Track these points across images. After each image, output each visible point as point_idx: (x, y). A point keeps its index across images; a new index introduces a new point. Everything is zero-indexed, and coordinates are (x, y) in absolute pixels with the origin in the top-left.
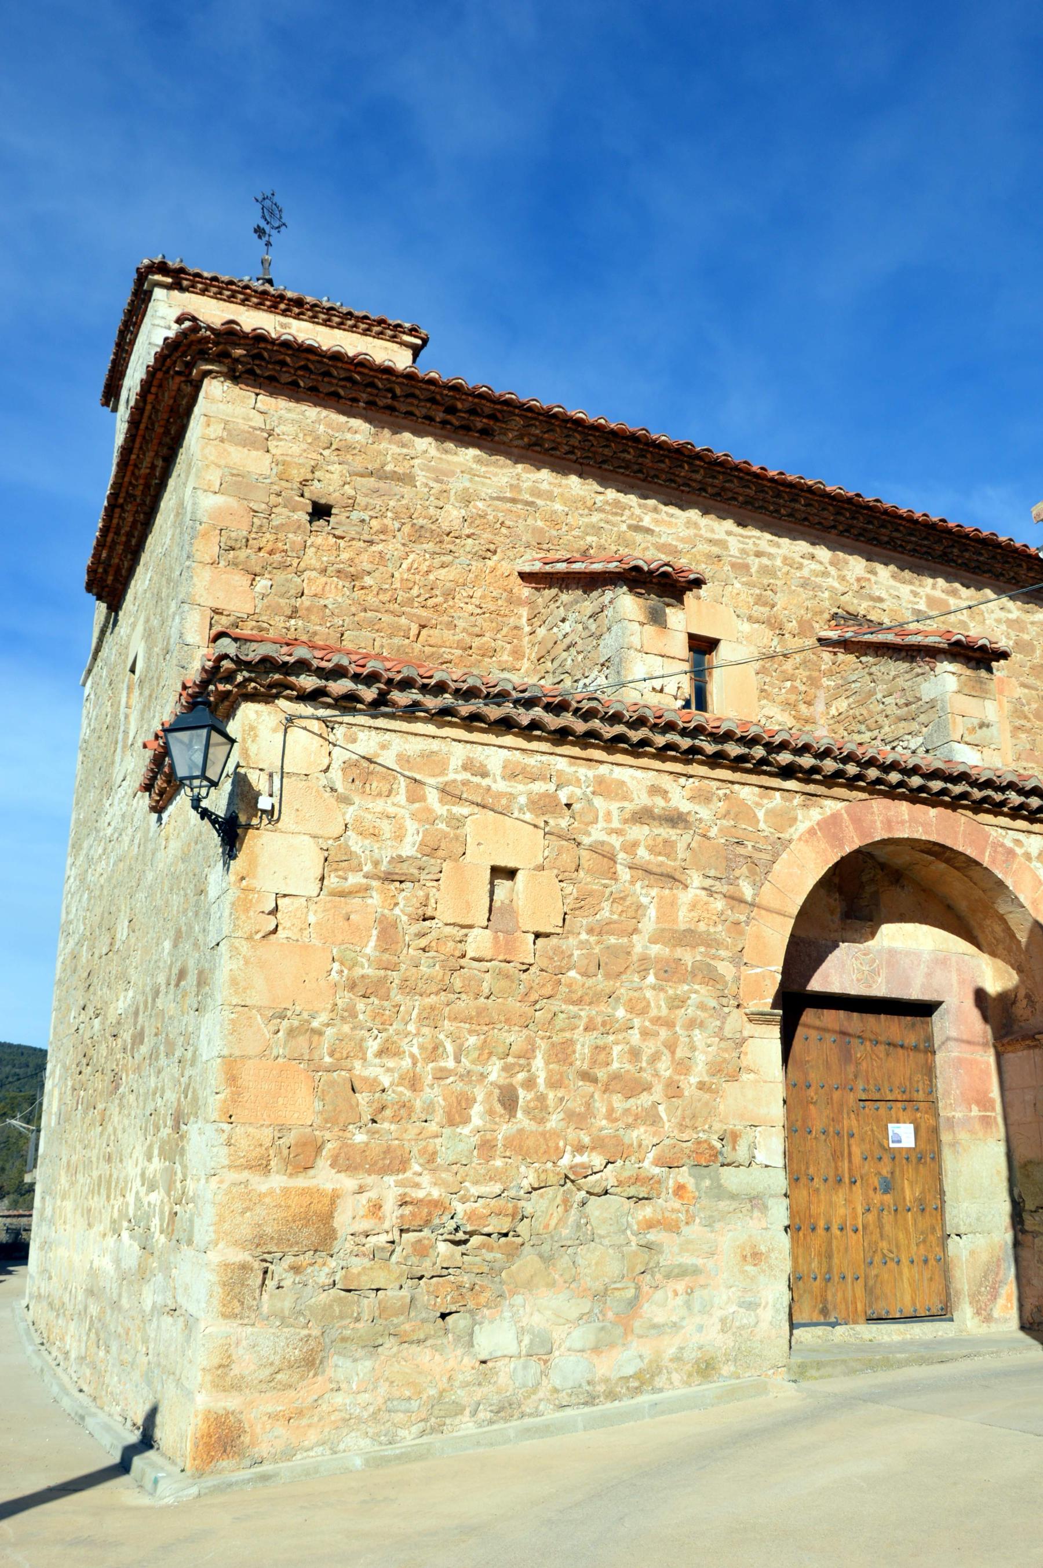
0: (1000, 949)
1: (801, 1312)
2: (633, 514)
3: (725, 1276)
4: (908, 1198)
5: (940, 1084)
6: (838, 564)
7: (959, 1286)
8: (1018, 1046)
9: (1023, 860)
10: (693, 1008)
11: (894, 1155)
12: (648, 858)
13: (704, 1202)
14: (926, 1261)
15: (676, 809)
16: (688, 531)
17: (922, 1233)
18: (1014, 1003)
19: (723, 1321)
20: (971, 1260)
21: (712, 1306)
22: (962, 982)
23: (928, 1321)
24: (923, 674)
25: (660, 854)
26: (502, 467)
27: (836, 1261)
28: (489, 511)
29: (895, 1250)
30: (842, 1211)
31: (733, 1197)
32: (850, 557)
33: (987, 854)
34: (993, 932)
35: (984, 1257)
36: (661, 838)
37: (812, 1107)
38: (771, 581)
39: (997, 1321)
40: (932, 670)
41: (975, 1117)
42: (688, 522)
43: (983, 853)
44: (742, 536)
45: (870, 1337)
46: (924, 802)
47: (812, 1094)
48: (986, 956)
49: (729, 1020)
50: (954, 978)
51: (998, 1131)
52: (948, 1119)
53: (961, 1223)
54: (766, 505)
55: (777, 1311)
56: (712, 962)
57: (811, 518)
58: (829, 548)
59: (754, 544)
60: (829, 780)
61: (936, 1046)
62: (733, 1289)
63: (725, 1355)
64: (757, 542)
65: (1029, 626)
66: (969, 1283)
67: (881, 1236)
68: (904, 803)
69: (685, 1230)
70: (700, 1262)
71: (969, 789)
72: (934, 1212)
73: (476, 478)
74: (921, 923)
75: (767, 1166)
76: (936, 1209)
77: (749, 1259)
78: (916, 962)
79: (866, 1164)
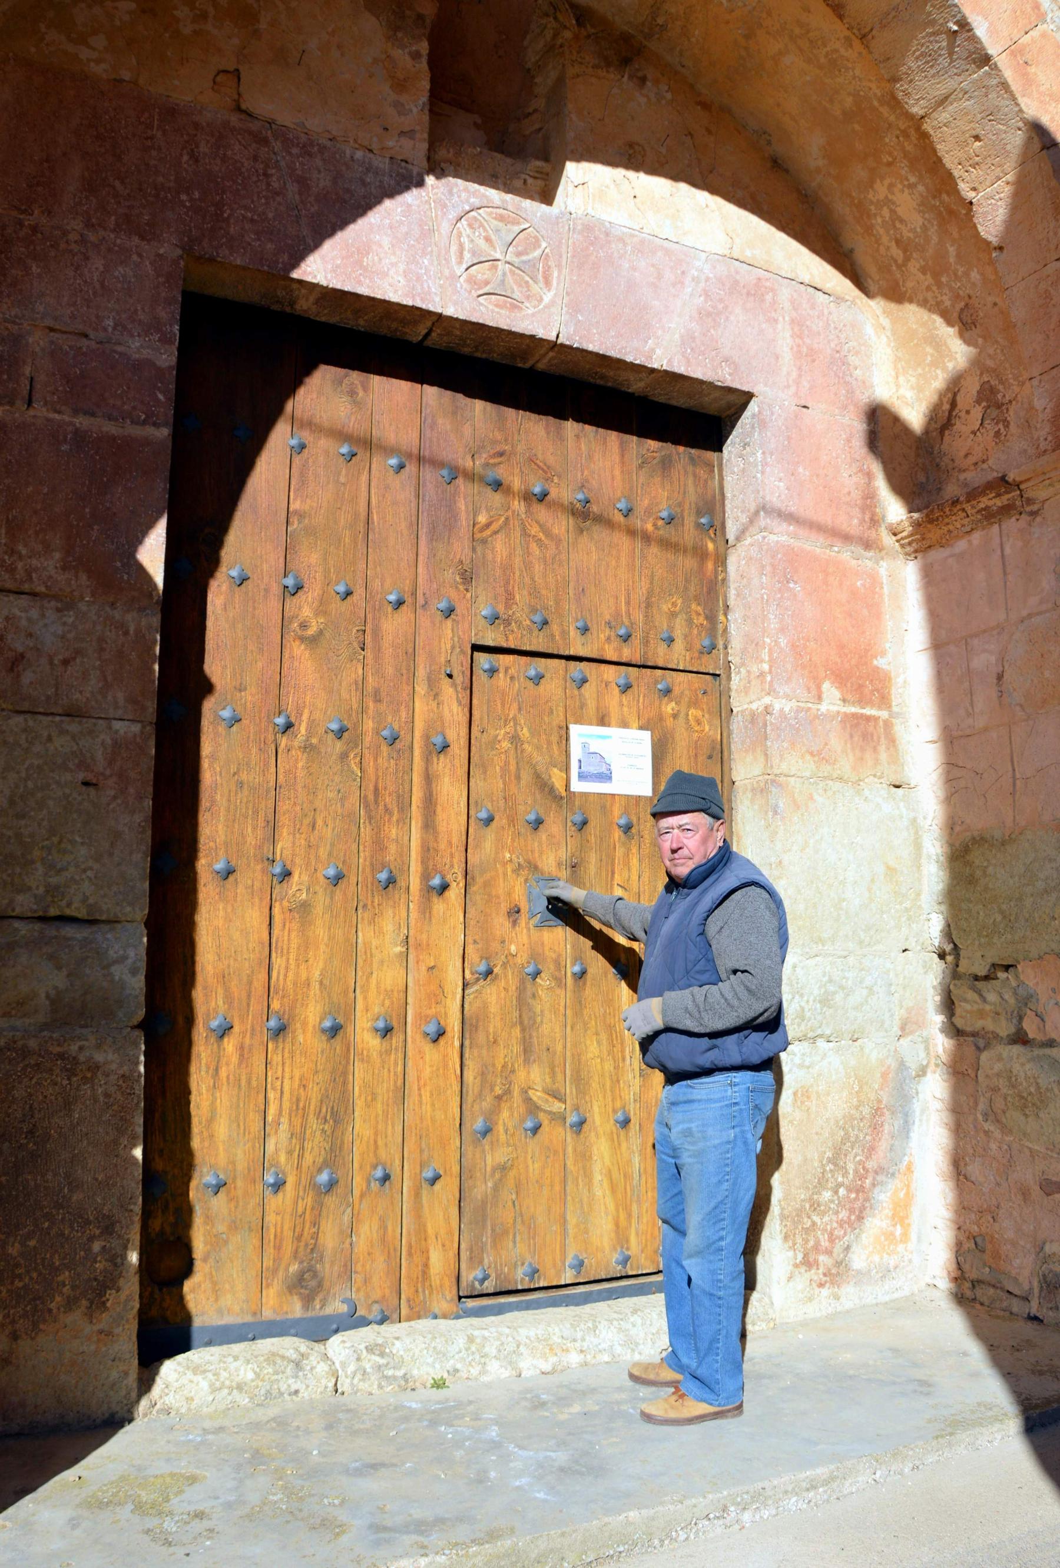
0: (915, 276)
1: (216, 1292)
8: (958, 522)
29: (570, 1090)
30: (390, 977)
37: (297, 649)
39: (862, 1277)
41: (830, 717)
45: (438, 1372)
47: (306, 612)
48: (877, 306)
50: (785, 342)
52: (753, 717)
61: (731, 532)
67: (527, 1050)
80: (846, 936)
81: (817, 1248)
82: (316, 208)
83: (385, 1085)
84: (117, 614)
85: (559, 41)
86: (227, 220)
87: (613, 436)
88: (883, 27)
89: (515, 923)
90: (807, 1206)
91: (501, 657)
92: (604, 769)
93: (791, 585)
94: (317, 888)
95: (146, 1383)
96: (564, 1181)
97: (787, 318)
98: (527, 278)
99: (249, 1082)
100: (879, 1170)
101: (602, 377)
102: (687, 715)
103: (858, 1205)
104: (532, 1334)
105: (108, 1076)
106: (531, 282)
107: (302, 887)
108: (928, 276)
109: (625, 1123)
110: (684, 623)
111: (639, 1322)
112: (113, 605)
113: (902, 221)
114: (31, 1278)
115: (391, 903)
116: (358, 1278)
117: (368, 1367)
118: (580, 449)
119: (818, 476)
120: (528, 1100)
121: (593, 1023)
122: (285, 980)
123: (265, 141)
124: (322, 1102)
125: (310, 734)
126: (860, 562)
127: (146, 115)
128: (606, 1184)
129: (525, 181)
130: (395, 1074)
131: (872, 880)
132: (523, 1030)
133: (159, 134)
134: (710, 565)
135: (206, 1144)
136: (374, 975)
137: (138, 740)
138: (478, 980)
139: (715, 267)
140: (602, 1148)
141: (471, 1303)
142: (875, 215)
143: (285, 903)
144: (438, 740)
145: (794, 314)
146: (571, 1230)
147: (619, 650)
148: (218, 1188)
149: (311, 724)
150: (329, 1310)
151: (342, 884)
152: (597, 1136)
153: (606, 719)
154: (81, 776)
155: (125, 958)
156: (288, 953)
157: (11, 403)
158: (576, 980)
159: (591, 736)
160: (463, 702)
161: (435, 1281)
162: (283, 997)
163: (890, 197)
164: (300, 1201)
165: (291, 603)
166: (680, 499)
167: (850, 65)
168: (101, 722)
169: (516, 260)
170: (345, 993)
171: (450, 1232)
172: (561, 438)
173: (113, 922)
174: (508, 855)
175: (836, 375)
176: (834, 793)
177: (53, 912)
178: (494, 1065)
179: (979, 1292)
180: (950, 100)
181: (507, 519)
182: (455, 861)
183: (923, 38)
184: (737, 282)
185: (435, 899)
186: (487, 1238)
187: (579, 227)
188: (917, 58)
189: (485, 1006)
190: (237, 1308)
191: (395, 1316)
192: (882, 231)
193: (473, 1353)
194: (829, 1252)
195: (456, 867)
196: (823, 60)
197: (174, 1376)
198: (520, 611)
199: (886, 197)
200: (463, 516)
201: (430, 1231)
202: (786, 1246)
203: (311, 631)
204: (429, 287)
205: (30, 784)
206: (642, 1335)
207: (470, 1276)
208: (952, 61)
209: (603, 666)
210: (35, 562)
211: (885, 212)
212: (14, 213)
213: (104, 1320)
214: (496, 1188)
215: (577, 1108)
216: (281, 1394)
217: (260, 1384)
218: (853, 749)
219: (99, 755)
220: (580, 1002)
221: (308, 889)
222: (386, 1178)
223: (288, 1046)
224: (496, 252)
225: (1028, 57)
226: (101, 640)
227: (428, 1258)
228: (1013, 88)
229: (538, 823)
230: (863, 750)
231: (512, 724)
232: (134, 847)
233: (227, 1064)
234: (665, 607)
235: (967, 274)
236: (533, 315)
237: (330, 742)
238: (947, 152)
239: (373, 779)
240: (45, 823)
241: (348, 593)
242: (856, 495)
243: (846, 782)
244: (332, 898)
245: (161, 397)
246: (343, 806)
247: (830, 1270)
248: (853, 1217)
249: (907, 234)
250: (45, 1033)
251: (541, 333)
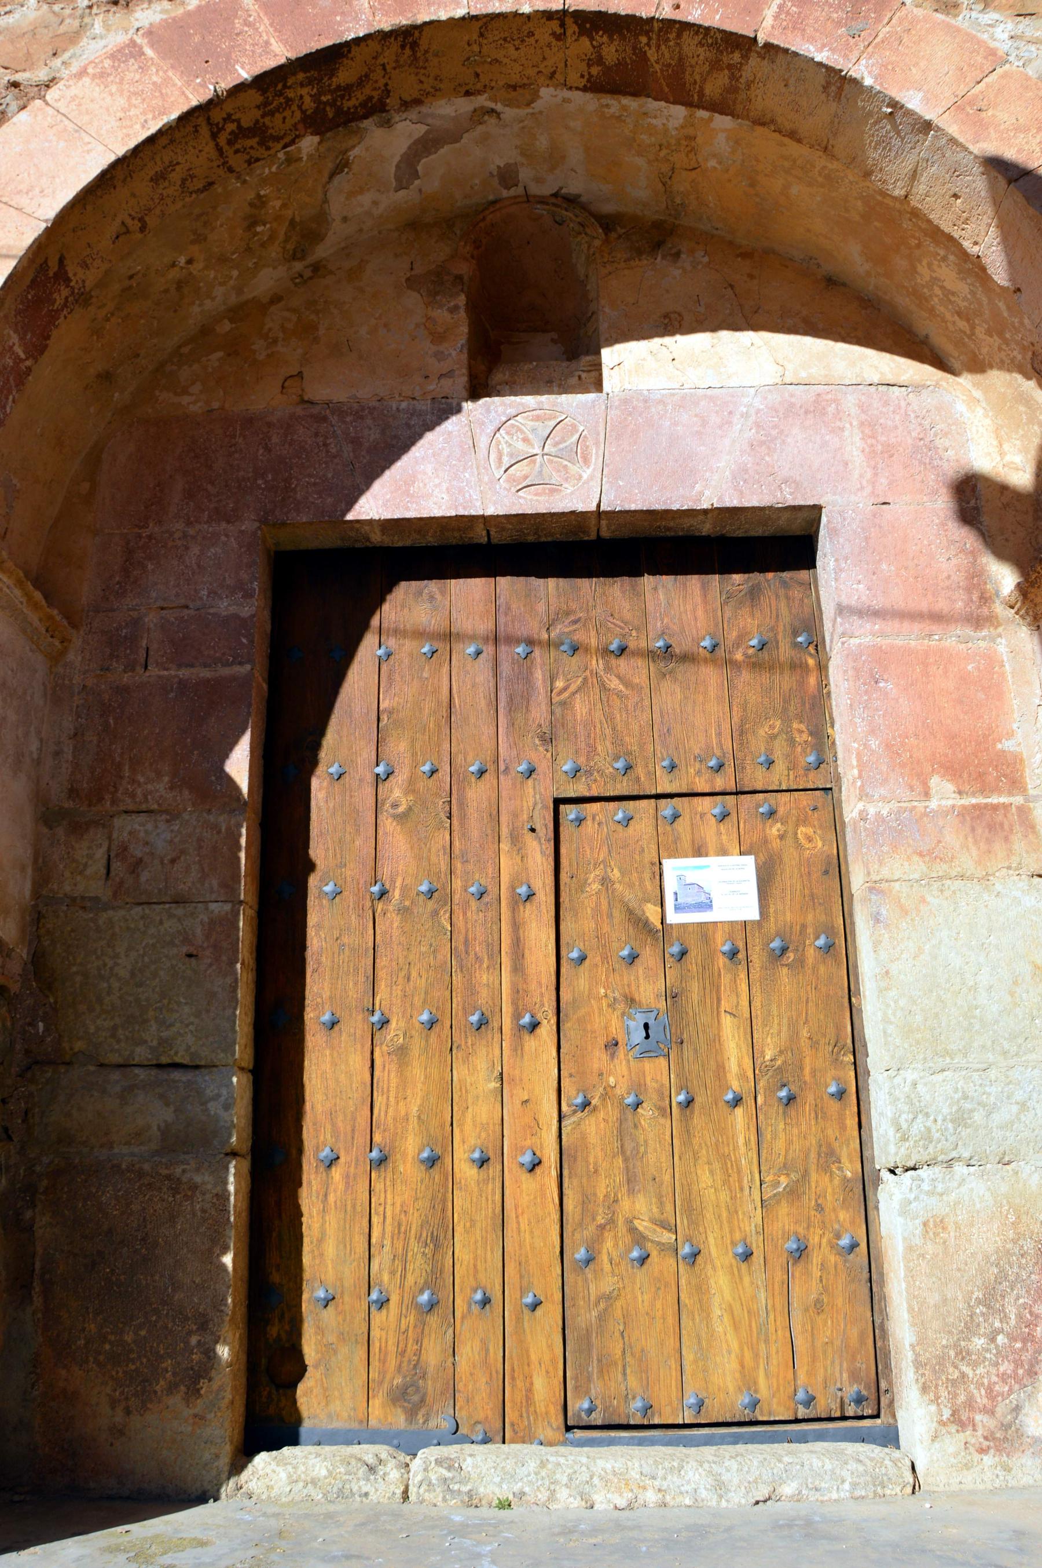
1: (327, 1399)
14: (801, 1253)
17: (786, 1168)
45: (505, 1492)
47: (397, 793)
48: (966, 380)
50: (854, 446)
67: (631, 1180)
72: (834, 1106)
76: (841, 1095)
80: (983, 1047)
82: (368, 458)
83: (483, 1212)
84: (212, 818)
85: (592, 251)
86: (294, 490)
88: (835, 135)
89: (613, 1056)
90: (952, 1353)
91: (588, 806)
92: (703, 898)
93: (881, 685)
94: (413, 1033)
95: (238, 1466)
97: (855, 423)
98: (566, 463)
99: (354, 1206)
101: (669, 529)
102: (796, 834)
103: (1026, 1357)
104: (609, 1466)
105: (204, 1194)
106: (569, 464)
107: (398, 1032)
108: (995, 337)
109: (747, 1256)
110: (784, 743)
111: (735, 1466)
113: (953, 294)
114: (142, 1363)
115: (484, 1042)
117: (433, 1478)
118: (659, 599)
119: (906, 568)
120: (633, 1230)
121: (704, 1152)
122: (386, 1115)
123: (325, 419)
124: (422, 1226)
125: (403, 895)
126: (970, 645)
127: (231, 429)
128: (726, 1319)
129: (580, 377)
130: (493, 1201)
131: (1015, 983)
132: (626, 1160)
133: (240, 440)
134: (812, 680)
135: (317, 1262)
136: (470, 1110)
137: (229, 916)
138: (575, 1112)
139: (766, 398)
140: (721, 1282)
141: (579, 1434)
142: (931, 296)
143: (384, 1048)
145: (863, 417)
147: (712, 781)
148: (327, 1302)
149: (404, 889)
151: (436, 1028)
152: (714, 1268)
153: (703, 850)
154: (185, 950)
155: (219, 1096)
156: (388, 1091)
157: (133, 670)
158: (681, 1110)
159: (686, 868)
160: (547, 853)
161: (541, 1408)
162: (385, 1131)
163: (934, 275)
164: (403, 1319)
166: (773, 623)
167: (842, 175)
168: (200, 905)
169: (553, 450)
171: (553, 1361)
172: (638, 594)
174: (602, 991)
175: (920, 462)
176: (954, 892)
177: (164, 1060)
178: (595, 1195)
180: (919, 172)
181: (585, 679)
182: (545, 1000)
183: (870, 129)
185: (526, 1037)
186: (593, 1367)
187: (617, 403)
188: (875, 148)
189: (584, 1137)
190: (345, 1415)
191: (500, 1438)
192: (942, 309)
193: (543, 1478)
195: (546, 1004)
196: (820, 179)
197: (262, 1465)
199: (931, 276)
201: (533, 1357)
202: (926, 1398)
203: (401, 809)
204: (470, 496)
205: (146, 959)
206: (736, 1481)
207: (578, 1405)
208: (903, 140)
209: (696, 799)
210: (149, 787)
211: (937, 291)
212: (137, 530)
213: (199, 1405)
216: (353, 1494)
217: (333, 1482)
218: (976, 842)
219: (199, 931)
220: (688, 1131)
221: (405, 1034)
223: (389, 1175)
224: (534, 448)
226: (200, 840)
227: (532, 1384)
228: (961, 140)
230: (988, 841)
231: (602, 866)
232: (227, 1004)
233: (335, 1191)
236: (572, 493)
237: (421, 903)
238: (940, 218)
239: (463, 931)
240: (157, 989)
242: (959, 578)
243: (971, 878)
244: (427, 1041)
245: (244, 641)
246: (435, 958)
247: (992, 1433)
248: (1021, 1372)
250: (156, 1158)
251: (580, 507)
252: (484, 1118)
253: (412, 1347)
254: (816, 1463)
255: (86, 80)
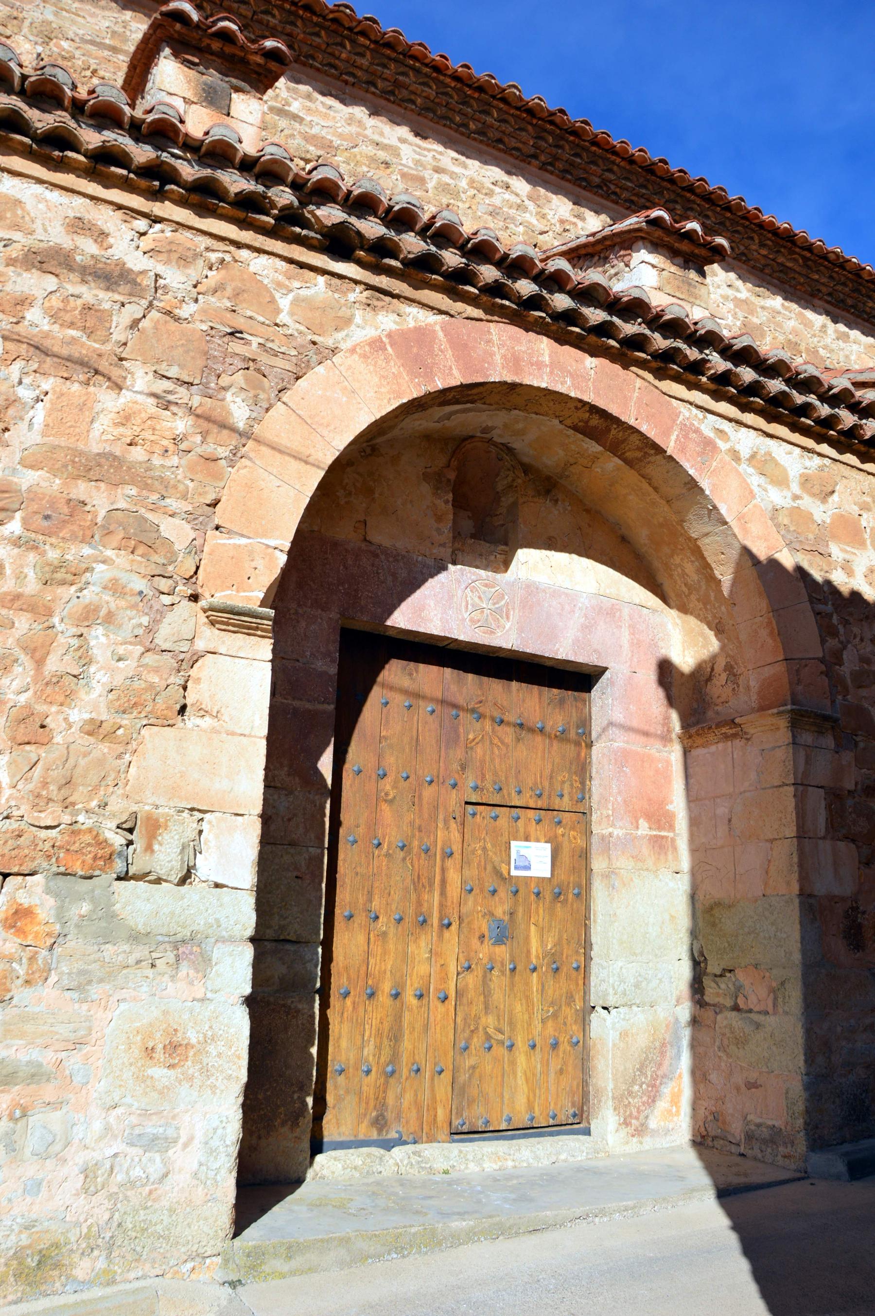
1: (338, 1124)
2: (277, 96)
3: (102, 1086)
4: (534, 952)
5: (596, 788)
6: (538, 199)
7: (601, 1083)
8: (711, 737)
9: (727, 458)
10: (97, 589)
11: (516, 888)
12: (46, 328)
13: (73, 943)
14: (555, 1046)
15: (121, 264)
16: (349, 128)
17: (552, 1004)
18: (709, 679)
19: (88, 1172)
20: (622, 1045)
21: (67, 1144)
22: (636, 644)
23: (551, 1134)
24: (616, 274)
25: (72, 325)
26: (103, 8)
27: (407, 1044)
28: (77, 54)
29: (506, 1029)
30: (422, 969)
31: (136, 937)
32: (554, 196)
33: (673, 437)
34: (684, 574)
35: (642, 1041)
36: (79, 302)
37: (385, 807)
38: (452, 201)
39: (654, 1133)
40: (627, 265)
41: (643, 837)
42: (350, 119)
43: (667, 433)
44: (419, 147)
45: (445, 1166)
46: (577, 343)
48: (674, 613)
49: (170, 617)
50: (625, 637)
51: (676, 858)
52: (603, 838)
53: (611, 991)
54: (450, 114)
55: (212, 1152)
56: (150, 516)
57: (506, 140)
58: (528, 181)
59: (434, 157)
60: (412, 271)
61: (594, 735)
62: (119, 1111)
63: (87, 1237)
64: (438, 156)
65: (759, 310)
66: (615, 1080)
67: (487, 1008)
68: (545, 339)
69: (22, 995)
70: (48, 1058)
71: (647, 332)
72: (574, 973)
73: (64, 13)
74: (580, 554)
75: (217, 886)
76: (577, 969)
77: (159, 1054)
78: (567, 607)
79: (471, 898)
81: (631, 1115)
84: (311, 796)
87: (535, 688)
89: (482, 942)
95: (311, 1163)
96: (503, 1076)
100: (664, 1076)
103: (652, 1094)
109: (534, 1047)
112: (309, 792)
116: (403, 1120)
141: (456, 1137)
144: (448, 851)
146: (506, 1101)
147: (536, 802)
148: (341, 1072)
149: (390, 843)
150: (389, 1136)
151: (402, 923)
154: (295, 874)
161: (440, 1123)
165: (382, 783)
169: (492, 607)
170: (402, 976)
173: (307, 943)
177: (282, 937)
179: (715, 1143)
184: (601, 608)
185: (445, 930)
186: (465, 1103)
189: (467, 985)
194: (637, 1118)
198: (488, 784)
200: (462, 735)
203: (390, 797)
210: (276, 772)
211: (679, 570)
214: (470, 1078)
215: (510, 1038)
222: (418, 1070)
225: (746, 519)
229: (494, 892)
230: (659, 854)
234: (559, 778)
235: (720, 607)
241: (408, 777)
249: (690, 582)
252: (422, 973)
253: (381, 1095)
254: (572, 1144)
255: (356, 357)
